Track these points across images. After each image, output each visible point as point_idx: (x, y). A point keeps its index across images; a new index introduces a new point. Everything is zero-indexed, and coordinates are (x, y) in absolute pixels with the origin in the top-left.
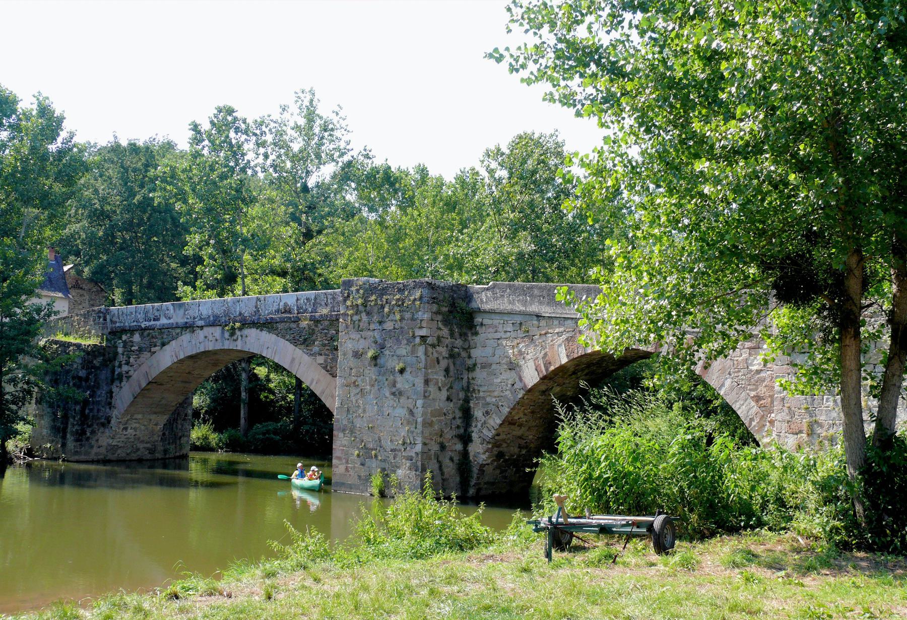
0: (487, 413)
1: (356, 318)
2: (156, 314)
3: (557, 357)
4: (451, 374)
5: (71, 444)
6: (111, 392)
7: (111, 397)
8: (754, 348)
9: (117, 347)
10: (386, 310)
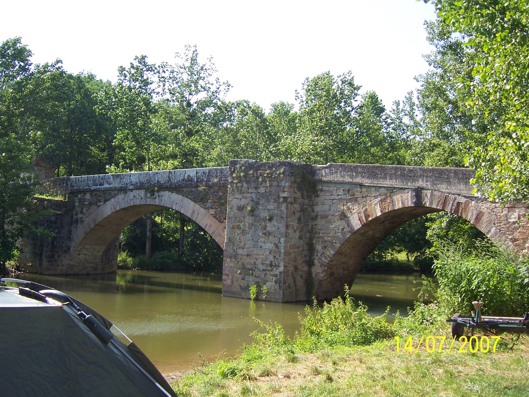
0: (325, 247)
1: (239, 185)
2: (101, 181)
3: (373, 212)
4: (302, 221)
5: (45, 263)
6: (71, 231)
7: (71, 234)
8: (512, 207)
9: (74, 202)
10: (260, 180)
